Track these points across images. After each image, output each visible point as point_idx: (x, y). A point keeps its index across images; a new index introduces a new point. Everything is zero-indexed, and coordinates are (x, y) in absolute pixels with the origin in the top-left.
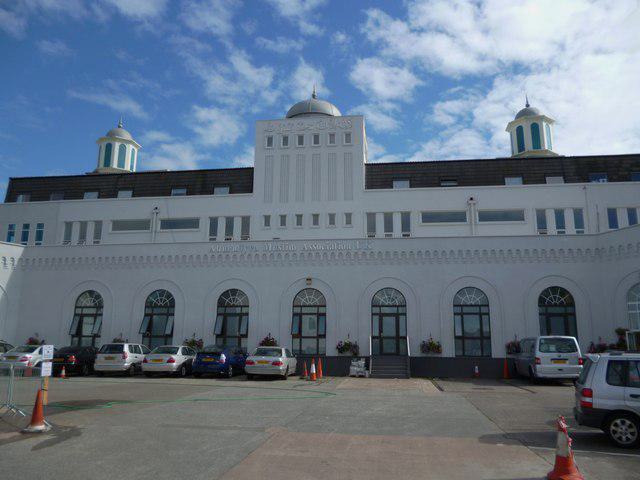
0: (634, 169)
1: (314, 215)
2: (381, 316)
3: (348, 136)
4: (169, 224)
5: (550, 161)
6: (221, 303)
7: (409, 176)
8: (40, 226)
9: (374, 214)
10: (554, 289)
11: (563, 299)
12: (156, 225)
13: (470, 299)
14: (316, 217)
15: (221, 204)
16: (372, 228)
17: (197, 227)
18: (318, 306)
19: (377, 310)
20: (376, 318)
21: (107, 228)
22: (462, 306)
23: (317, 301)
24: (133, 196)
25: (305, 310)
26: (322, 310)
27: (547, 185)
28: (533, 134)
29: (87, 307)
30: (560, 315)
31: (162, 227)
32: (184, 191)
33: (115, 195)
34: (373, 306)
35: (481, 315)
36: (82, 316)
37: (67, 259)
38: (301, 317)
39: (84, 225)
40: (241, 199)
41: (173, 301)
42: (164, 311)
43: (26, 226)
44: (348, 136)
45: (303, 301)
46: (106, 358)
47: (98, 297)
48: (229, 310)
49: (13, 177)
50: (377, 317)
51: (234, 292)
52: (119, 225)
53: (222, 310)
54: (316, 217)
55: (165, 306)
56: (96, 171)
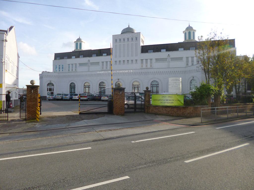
1: (115, 61)
2: (71, 88)
3: (136, 38)
5: (180, 44)
6: (100, 85)
8: (63, 65)
9: (107, 62)
13: (154, 83)
15: (104, 58)
16: (187, 61)
19: (152, 86)
20: (100, 88)
21: (78, 65)
23: (156, 84)
24: (166, 51)
25: (154, 86)
26: (158, 86)
28: (189, 35)
29: (154, 85)
30: (137, 87)
32: (106, 54)
34: (133, 85)
35: (157, 87)
36: (71, 88)
37: (138, 73)
40: (109, 57)
41: (75, 85)
43: (59, 66)
44: (136, 38)
45: (153, 84)
46: (12, 98)
47: (50, 83)
48: (102, 86)
51: (102, 82)
53: (71, 87)
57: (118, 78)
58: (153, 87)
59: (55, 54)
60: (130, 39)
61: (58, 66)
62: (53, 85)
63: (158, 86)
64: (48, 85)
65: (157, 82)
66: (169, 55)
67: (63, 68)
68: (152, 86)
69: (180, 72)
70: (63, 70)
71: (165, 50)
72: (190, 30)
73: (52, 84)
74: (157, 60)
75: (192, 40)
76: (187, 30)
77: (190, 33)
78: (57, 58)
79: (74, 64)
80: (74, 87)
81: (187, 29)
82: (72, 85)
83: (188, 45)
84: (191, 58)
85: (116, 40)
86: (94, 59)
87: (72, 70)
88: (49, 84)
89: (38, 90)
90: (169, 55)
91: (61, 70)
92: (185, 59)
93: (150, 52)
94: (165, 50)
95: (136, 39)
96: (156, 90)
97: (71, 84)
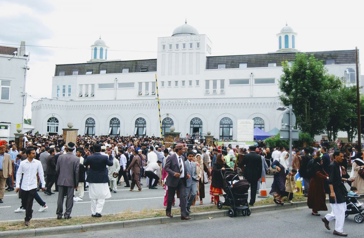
0: (328, 58)
2: (88, 127)
4: (122, 85)
7: (246, 61)
8: (70, 86)
9: (216, 80)
10: (197, 118)
11: (199, 122)
12: (252, 82)
14: (190, 82)
17: (248, 83)
18: (230, 124)
19: (222, 126)
21: (227, 83)
22: (223, 124)
23: (229, 122)
24: (107, 73)
25: (224, 126)
26: (262, 126)
27: (218, 69)
31: (255, 83)
32: (91, 73)
33: (121, 72)
34: (220, 124)
38: (93, 128)
39: (215, 82)
41: (119, 122)
42: (117, 125)
43: (64, 86)
47: (53, 118)
49: (57, 64)
50: (222, 128)
52: (101, 86)
54: (190, 82)
55: (92, 124)
56: (91, 61)
57: (167, 113)
58: (223, 128)
59: (57, 66)
60: (188, 46)
61: (61, 88)
62: (57, 122)
63: (262, 126)
64: (49, 121)
65: (230, 119)
66: (252, 73)
67: (70, 90)
68: (222, 126)
69: (270, 104)
70: (69, 95)
71: (246, 65)
72: (103, 46)
73: (56, 119)
74: (233, 82)
75: (291, 49)
76: (282, 33)
77: (287, 37)
78: (60, 73)
79: (85, 85)
80: (92, 125)
81: (283, 31)
82: (115, 121)
83: (283, 58)
84: (151, 83)
85: (164, 46)
86: (126, 76)
87: (214, 91)
88: (50, 119)
89: (281, 137)
90: (252, 73)
91: (67, 93)
92: (137, 86)
93: (330, 64)
94: (246, 65)
95: (198, 46)
96: (166, 129)
97: (87, 119)
